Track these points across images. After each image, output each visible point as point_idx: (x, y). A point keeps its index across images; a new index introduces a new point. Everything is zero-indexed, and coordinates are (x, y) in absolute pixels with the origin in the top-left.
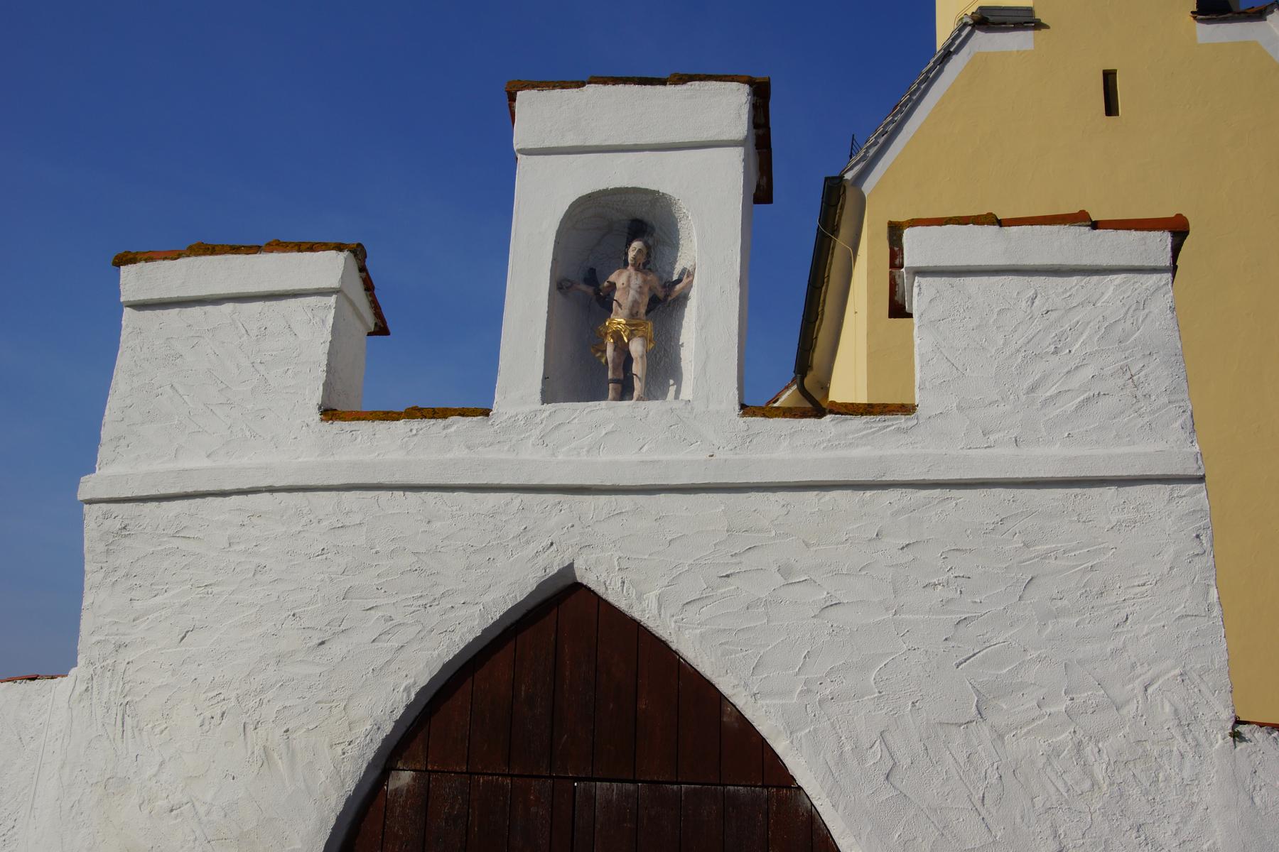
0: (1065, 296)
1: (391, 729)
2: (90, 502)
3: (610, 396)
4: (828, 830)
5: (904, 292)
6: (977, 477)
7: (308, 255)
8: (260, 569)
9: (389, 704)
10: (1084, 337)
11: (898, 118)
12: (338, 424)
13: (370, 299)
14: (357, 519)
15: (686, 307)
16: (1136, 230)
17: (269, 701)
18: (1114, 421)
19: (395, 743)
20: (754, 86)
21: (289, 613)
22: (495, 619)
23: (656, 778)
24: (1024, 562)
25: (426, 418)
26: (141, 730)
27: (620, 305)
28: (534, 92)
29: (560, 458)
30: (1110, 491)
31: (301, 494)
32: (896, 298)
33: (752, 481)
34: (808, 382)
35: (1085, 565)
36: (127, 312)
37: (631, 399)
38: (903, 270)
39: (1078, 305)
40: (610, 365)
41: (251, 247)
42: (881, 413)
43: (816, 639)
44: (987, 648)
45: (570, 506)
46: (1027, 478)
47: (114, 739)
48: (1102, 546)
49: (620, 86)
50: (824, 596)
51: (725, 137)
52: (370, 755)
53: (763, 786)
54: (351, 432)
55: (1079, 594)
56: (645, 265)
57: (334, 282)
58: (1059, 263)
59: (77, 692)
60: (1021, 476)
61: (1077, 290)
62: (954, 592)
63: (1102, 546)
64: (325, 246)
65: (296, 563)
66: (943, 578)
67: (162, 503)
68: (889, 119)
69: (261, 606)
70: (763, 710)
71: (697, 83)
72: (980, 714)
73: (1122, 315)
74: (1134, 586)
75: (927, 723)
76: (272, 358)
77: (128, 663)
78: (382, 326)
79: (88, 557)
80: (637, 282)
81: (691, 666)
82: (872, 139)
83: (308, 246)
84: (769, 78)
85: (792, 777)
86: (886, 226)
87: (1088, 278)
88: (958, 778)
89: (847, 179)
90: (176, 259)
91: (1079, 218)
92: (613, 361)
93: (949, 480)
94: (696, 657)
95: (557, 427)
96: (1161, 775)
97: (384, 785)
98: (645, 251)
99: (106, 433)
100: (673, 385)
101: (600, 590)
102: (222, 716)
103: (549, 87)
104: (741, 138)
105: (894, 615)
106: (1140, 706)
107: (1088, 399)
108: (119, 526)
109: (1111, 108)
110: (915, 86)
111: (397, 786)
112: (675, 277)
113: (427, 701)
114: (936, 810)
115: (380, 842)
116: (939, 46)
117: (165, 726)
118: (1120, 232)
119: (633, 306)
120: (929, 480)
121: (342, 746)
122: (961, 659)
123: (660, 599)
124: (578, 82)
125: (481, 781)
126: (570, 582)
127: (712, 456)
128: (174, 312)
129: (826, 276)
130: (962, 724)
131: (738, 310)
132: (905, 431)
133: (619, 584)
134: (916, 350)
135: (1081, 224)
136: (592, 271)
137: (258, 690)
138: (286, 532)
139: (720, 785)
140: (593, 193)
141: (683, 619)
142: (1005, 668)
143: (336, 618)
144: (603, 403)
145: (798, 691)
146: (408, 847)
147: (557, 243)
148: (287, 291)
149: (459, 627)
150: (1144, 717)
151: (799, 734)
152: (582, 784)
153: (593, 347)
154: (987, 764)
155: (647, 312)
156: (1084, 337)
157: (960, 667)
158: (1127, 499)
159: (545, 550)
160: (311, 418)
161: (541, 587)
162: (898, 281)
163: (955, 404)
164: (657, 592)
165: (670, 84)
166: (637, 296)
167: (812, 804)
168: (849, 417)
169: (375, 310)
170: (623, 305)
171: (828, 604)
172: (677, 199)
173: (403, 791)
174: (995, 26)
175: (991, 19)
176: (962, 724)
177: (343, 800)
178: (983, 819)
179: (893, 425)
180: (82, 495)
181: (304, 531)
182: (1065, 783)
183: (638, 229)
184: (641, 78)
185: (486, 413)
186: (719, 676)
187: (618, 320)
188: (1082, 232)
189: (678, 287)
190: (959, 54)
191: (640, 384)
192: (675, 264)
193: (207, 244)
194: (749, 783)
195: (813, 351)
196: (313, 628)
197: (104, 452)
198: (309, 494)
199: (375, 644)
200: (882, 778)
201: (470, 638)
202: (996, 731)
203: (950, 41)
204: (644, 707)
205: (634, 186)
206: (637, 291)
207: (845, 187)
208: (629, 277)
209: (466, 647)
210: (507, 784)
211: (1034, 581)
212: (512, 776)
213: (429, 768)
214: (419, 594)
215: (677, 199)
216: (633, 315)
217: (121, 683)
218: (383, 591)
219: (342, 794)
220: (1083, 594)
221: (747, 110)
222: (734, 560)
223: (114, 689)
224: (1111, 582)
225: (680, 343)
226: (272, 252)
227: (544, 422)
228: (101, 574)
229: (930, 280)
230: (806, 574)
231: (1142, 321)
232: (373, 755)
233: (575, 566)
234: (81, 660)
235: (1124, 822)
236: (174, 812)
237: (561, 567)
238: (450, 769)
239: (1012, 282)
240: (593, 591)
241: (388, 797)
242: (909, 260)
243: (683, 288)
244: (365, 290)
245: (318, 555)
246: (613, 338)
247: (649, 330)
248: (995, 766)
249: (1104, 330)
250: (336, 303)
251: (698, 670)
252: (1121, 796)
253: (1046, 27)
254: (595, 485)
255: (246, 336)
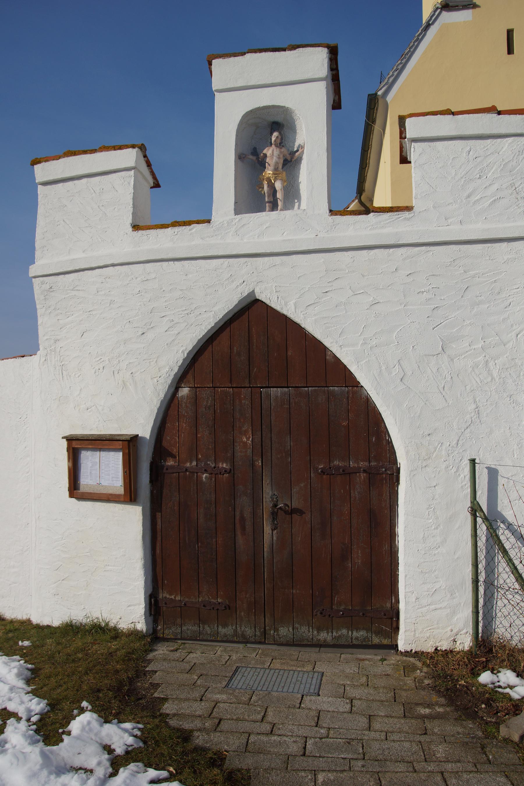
0: (484, 150)
1: (177, 370)
2: (35, 277)
3: (267, 210)
4: (375, 404)
5: (407, 150)
6: (443, 240)
7: (119, 152)
8: (112, 302)
9: (175, 359)
10: (493, 170)
11: (404, 61)
12: (141, 232)
13: (150, 170)
14: (153, 276)
15: (301, 164)
16: (519, 114)
17: (123, 361)
18: (507, 211)
19: (180, 376)
20: (330, 49)
21: (127, 321)
22: (220, 318)
23: (297, 385)
24: (464, 280)
25: (181, 226)
26: (70, 376)
27: (269, 165)
28: (221, 60)
29: (245, 241)
30: (504, 245)
31: (127, 266)
32: (403, 154)
33: (336, 247)
34: (363, 198)
35: (492, 280)
36: (40, 187)
37: (277, 210)
38: (406, 140)
39: (491, 154)
40: (266, 195)
41: (92, 150)
42: (397, 211)
43: (368, 319)
44: (446, 320)
45: (251, 264)
46: (466, 240)
47: (60, 381)
48: (500, 271)
49: (263, 53)
50: (371, 300)
51: (317, 76)
52: (169, 382)
53: (346, 387)
54: (147, 235)
55: (489, 294)
56: (280, 144)
57: (132, 164)
58: (482, 133)
59: (41, 362)
60: (463, 239)
61: (490, 146)
62: (432, 295)
63: (500, 271)
64: (126, 147)
65: (128, 298)
66: (426, 289)
67: (65, 275)
68: (399, 62)
69: (115, 319)
70: (345, 353)
71: (301, 49)
72: (443, 350)
73: (512, 158)
74: (514, 289)
75: (419, 355)
76: (107, 203)
77: (61, 348)
78: (157, 183)
79: (37, 302)
80: (277, 153)
81: (311, 334)
82: (391, 73)
83: (119, 147)
84: (337, 44)
85: (359, 382)
86: (398, 118)
87: (496, 140)
88: (433, 379)
89: (379, 95)
90: (58, 159)
91: (492, 110)
92: (268, 192)
93: (429, 242)
94: (313, 330)
95: (242, 226)
96: (521, 373)
97: (176, 394)
98: (280, 137)
99: (37, 245)
100: (297, 202)
101: (267, 302)
102: (103, 368)
103: (228, 56)
104: (325, 76)
105: (404, 307)
106: (514, 343)
107: (495, 200)
108: (48, 287)
109: (510, 50)
110: (412, 44)
111: (182, 395)
112: (295, 149)
113: (192, 357)
114: (423, 393)
115: (177, 418)
116: (424, 21)
117: (79, 374)
118: (511, 116)
119: (276, 165)
120: (420, 242)
121: (157, 378)
122: (435, 326)
123: (295, 304)
124: (242, 53)
125: (219, 390)
126: (253, 299)
127: (317, 236)
128: (60, 185)
129: (370, 145)
130: (435, 355)
131: (326, 163)
132: (409, 219)
133: (276, 298)
134: (413, 179)
135: (493, 112)
136: (255, 149)
137: (117, 356)
138: (122, 284)
139: (326, 387)
140: (253, 110)
141: (306, 313)
142: (455, 329)
143: (148, 322)
144: (264, 213)
145: (361, 343)
146: (190, 420)
147: (237, 136)
148: (111, 170)
149: (204, 322)
150: (516, 348)
151: (361, 363)
152: (264, 390)
153: (257, 186)
154: (446, 372)
155: (282, 168)
156: (493, 170)
157: (434, 329)
158: (512, 248)
159: (241, 284)
160: (128, 230)
161: (240, 302)
162: (404, 145)
163: (432, 205)
164: (294, 301)
165: (288, 51)
166: (277, 160)
167: (368, 393)
168: (381, 213)
169: (153, 176)
170: (271, 165)
171: (373, 303)
172: (294, 109)
173: (185, 396)
174: (453, 8)
175: (451, 4)
176: (435, 355)
177: (159, 402)
178: (444, 396)
179: (402, 217)
180: (31, 274)
181: (130, 283)
182: (480, 379)
183: (276, 126)
184: (273, 48)
185: (209, 221)
186: (324, 338)
187: (269, 172)
188: (494, 116)
189: (297, 154)
190: (434, 25)
191: (281, 203)
192: (295, 142)
193: (72, 151)
194: (339, 386)
195: (365, 183)
196: (138, 327)
197: (38, 254)
198: (130, 266)
199: (167, 332)
200: (399, 380)
201: (209, 327)
202: (450, 357)
203: (430, 18)
204: (290, 354)
205: (273, 104)
206: (277, 157)
207: (378, 99)
208: (273, 151)
209: (208, 331)
210: (231, 391)
211: (469, 288)
212: (233, 387)
213: (196, 386)
214: (185, 309)
215: (294, 109)
216: (276, 169)
217: (59, 356)
218: (168, 308)
219: (159, 399)
220: (491, 293)
221: (327, 61)
222: (329, 285)
223: (56, 359)
224: (503, 287)
225: (299, 182)
226: (102, 152)
227: (237, 224)
228: (44, 309)
229: (419, 144)
230: (363, 289)
231: (521, 161)
232: (170, 381)
233: (255, 291)
234: (41, 347)
235: (504, 395)
236: (89, 410)
237: (249, 292)
238: (205, 386)
239: (459, 143)
240: (264, 303)
241: (179, 399)
242: (409, 134)
243: (299, 154)
244: (147, 166)
245: (137, 294)
246: (267, 181)
247: (284, 176)
248: (449, 373)
249: (503, 166)
250: (134, 174)
251: (314, 336)
252: (504, 383)
253: (478, 6)
254: (262, 253)
255: (94, 193)
